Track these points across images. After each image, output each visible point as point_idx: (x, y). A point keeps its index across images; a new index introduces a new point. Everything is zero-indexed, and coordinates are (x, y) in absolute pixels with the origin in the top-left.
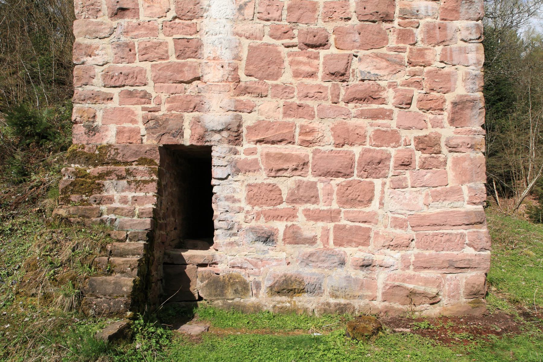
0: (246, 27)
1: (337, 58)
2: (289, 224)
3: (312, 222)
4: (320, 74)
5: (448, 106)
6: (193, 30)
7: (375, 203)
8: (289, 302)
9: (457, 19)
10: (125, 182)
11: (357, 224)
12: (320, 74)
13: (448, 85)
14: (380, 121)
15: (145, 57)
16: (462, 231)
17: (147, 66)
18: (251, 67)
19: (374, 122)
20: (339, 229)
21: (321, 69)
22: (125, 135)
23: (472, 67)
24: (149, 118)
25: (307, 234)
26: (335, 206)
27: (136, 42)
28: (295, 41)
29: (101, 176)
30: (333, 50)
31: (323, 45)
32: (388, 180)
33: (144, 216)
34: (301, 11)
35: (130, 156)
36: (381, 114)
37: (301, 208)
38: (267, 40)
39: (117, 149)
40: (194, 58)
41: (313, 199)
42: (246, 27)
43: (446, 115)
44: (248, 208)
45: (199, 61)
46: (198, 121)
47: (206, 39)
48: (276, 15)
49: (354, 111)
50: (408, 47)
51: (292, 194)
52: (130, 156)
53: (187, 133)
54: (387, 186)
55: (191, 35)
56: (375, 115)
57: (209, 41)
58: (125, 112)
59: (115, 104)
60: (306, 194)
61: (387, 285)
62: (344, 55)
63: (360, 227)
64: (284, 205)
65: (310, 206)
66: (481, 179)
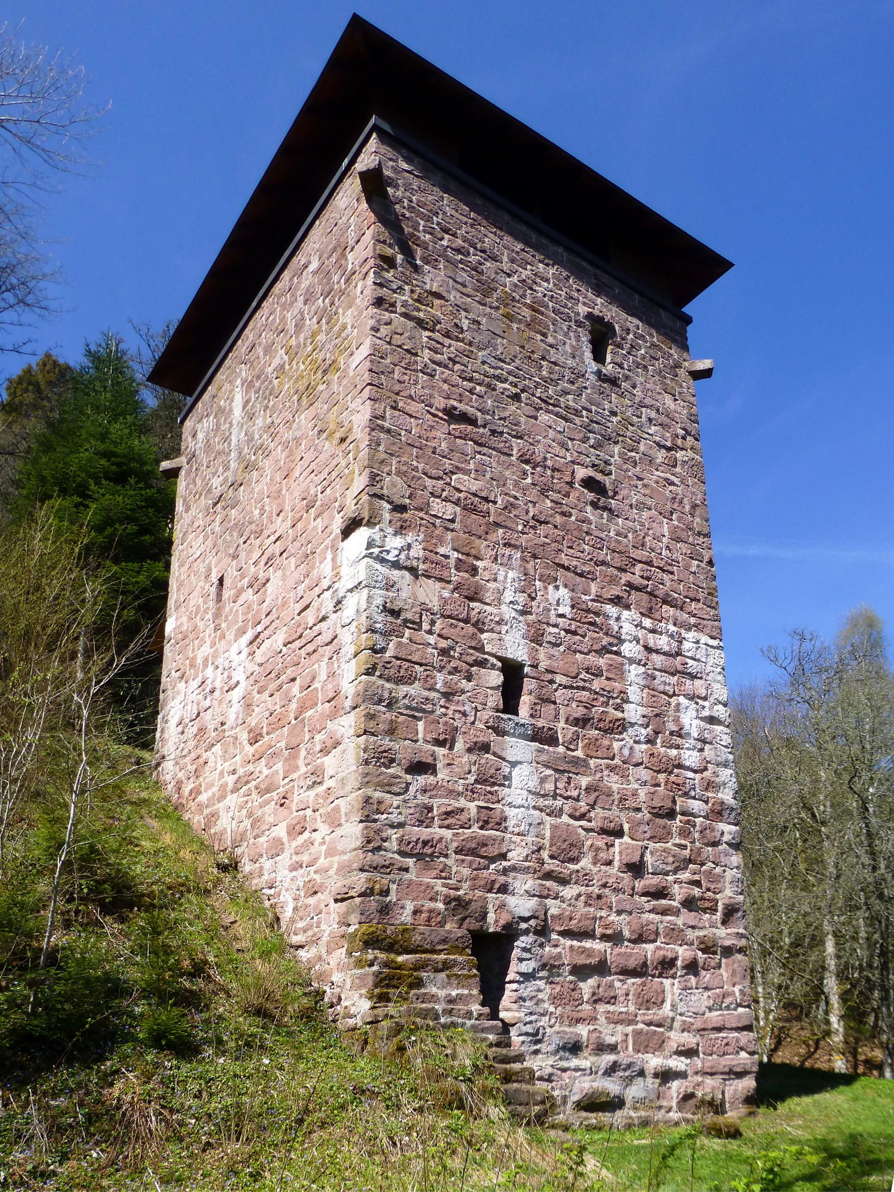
0: (547, 803)
1: (634, 848)
2: (591, 1028)
3: (612, 1026)
4: (616, 864)
5: (720, 907)
6: (495, 799)
7: (667, 1005)
8: (596, 1119)
9: (721, 821)
10: (443, 975)
11: (652, 1028)
12: (616, 864)
13: (719, 886)
14: (669, 918)
15: (447, 822)
16: (737, 1034)
17: (448, 834)
18: (554, 848)
19: (664, 917)
20: (638, 1033)
21: (617, 858)
22: (423, 915)
23: (735, 870)
24: (452, 897)
25: (610, 1040)
26: (632, 1008)
27: (436, 803)
28: (592, 825)
29: (419, 966)
30: (626, 839)
31: (619, 833)
32: (676, 981)
33: (482, 1017)
34: (596, 794)
35: (439, 943)
36: (668, 910)
37: (602, 1008)
38: (565, 818)
39: (423, 934)
40: (497, 830)
41: (613, 1000)
42: (547, 803)
43: (719, 914)
44: (552, 1009)
45: (502, 834)
46: (502, 906)
47: (510, 812)
48: (575, 793)
49: (648, 907)
50: (689, 844)
51: (594, 994)
52: (439, 943)
53: (491, 917)
54: (676, 987)
55: (493, 803)
56: (664, 912)
57: (512, 814)
58: (423, 887)
59: (411, 876)
60: (606, 994)
61: (679, 1094)
62: (637, 846)
63: (655, 1031)
64: (586, 1007)
65: (611, 1008)
66: (385, 939)
